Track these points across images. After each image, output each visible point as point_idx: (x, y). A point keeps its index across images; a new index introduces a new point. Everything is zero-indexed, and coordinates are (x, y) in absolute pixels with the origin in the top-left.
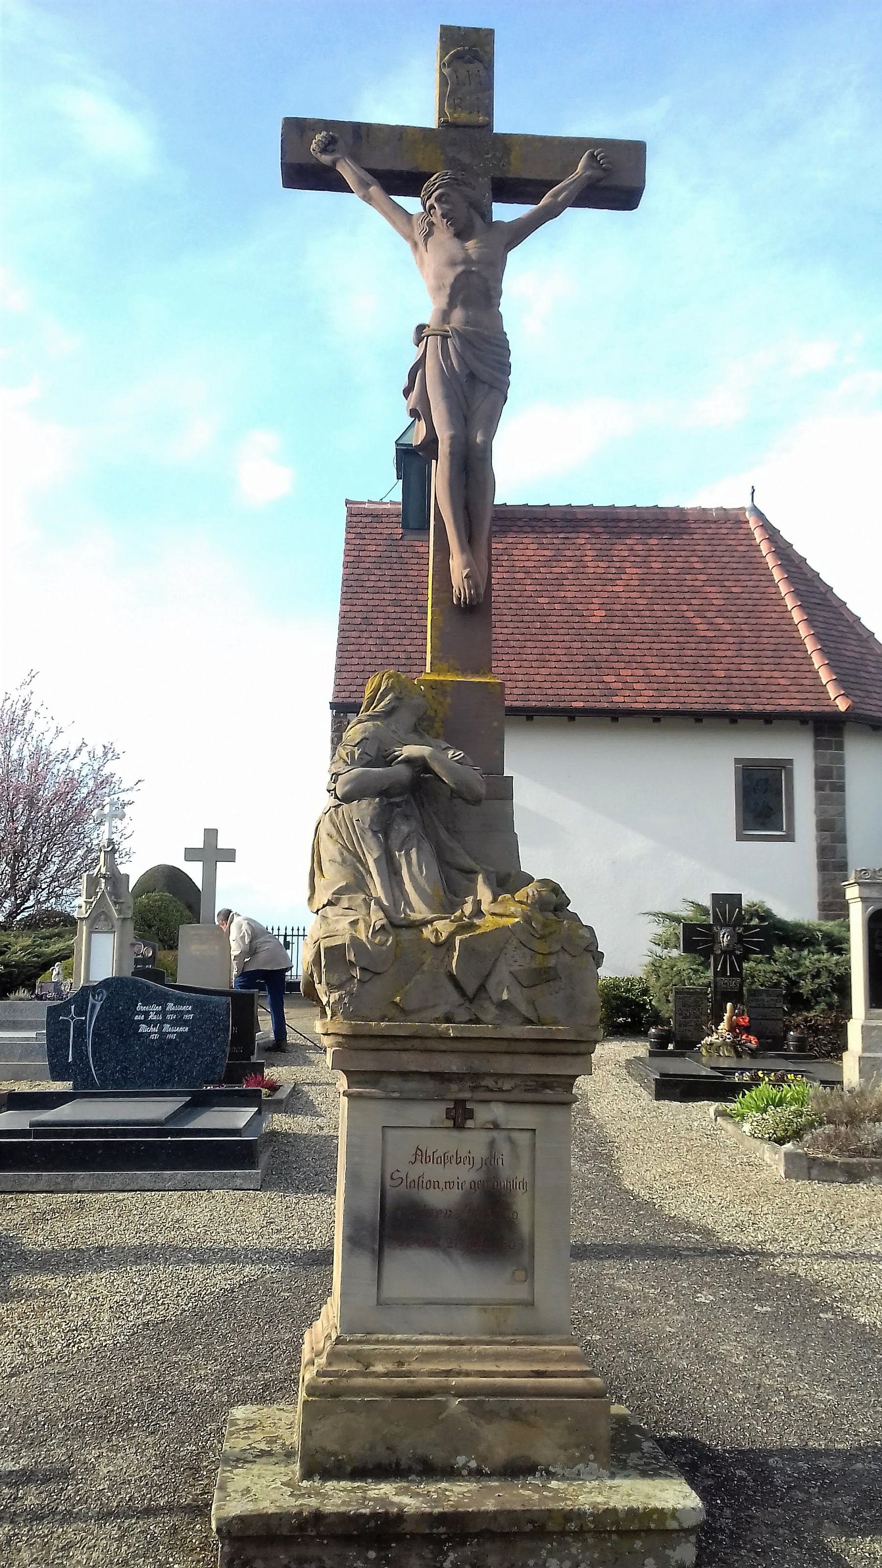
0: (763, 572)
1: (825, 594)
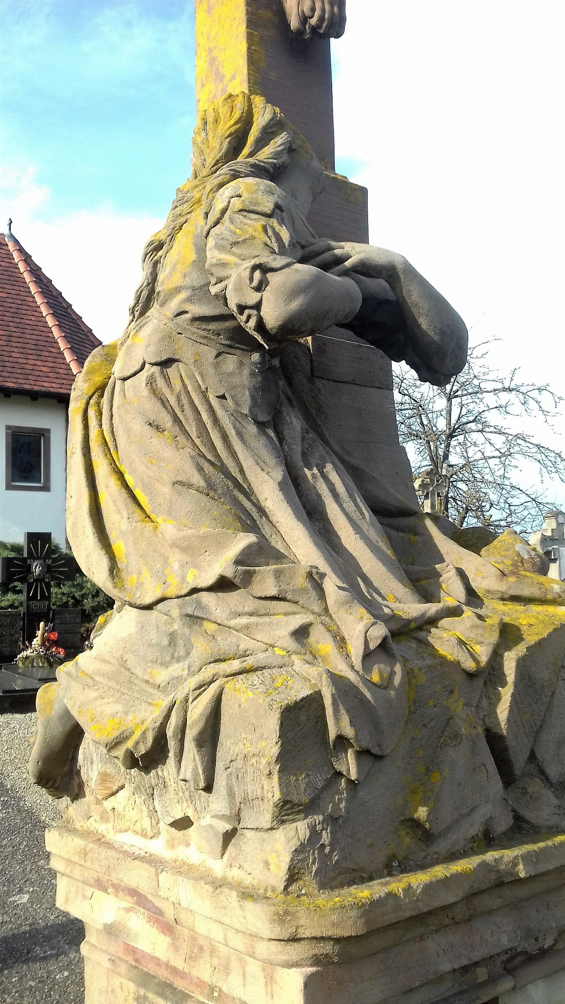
0: (22, 284)
1: (67, 309)
